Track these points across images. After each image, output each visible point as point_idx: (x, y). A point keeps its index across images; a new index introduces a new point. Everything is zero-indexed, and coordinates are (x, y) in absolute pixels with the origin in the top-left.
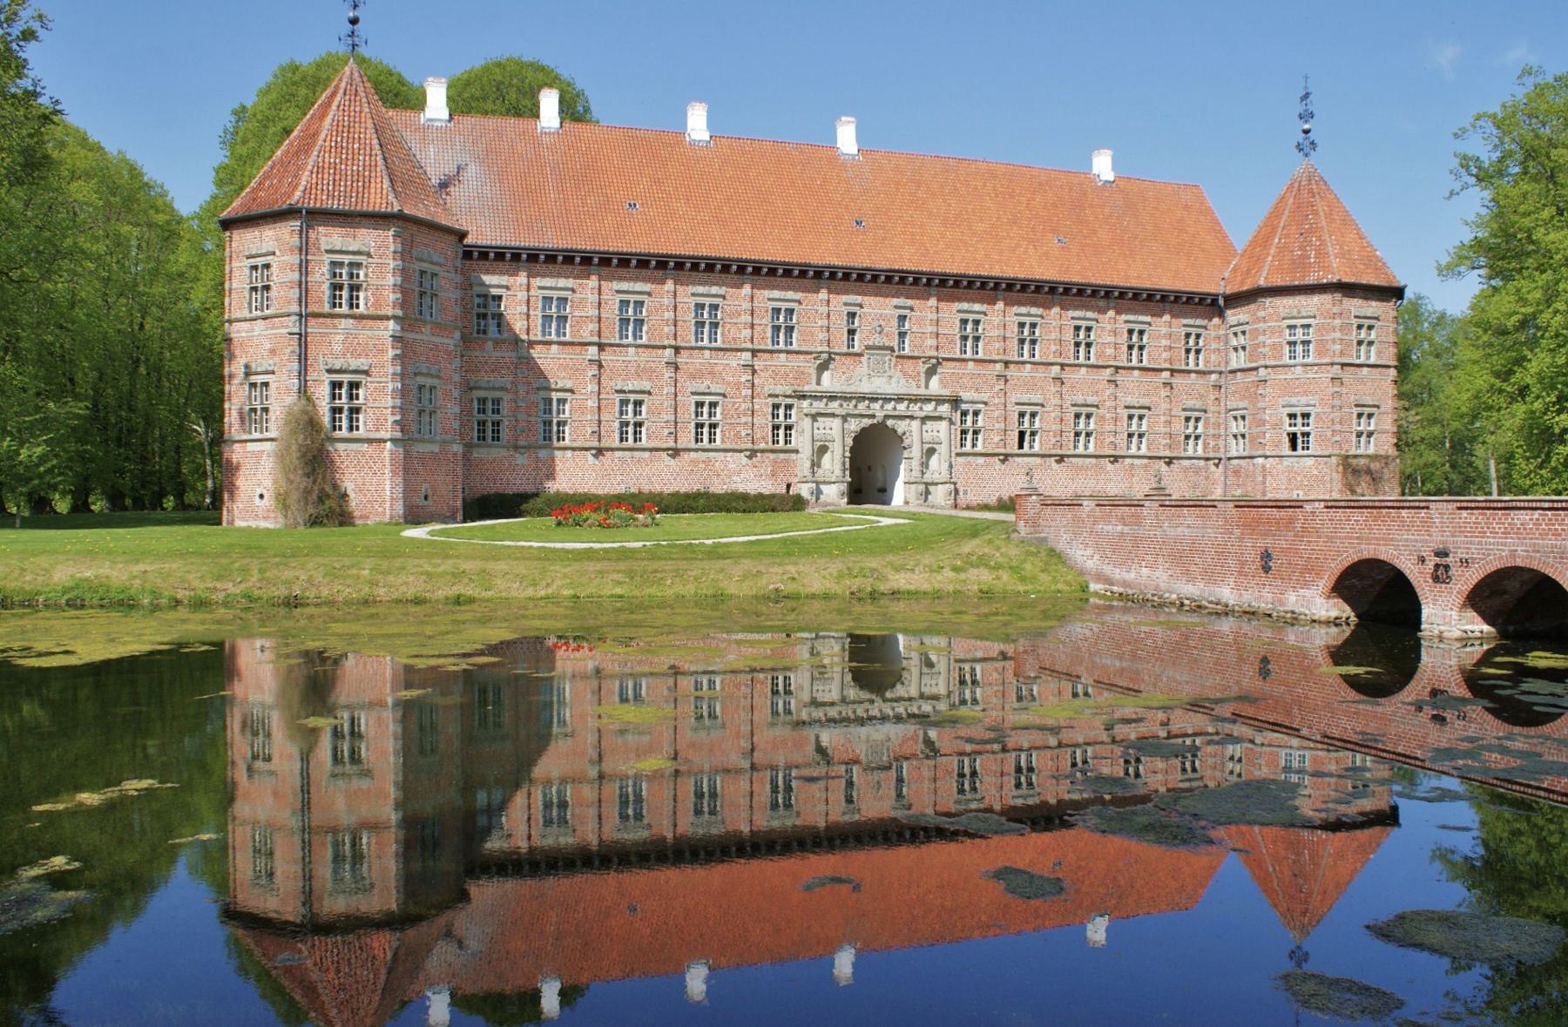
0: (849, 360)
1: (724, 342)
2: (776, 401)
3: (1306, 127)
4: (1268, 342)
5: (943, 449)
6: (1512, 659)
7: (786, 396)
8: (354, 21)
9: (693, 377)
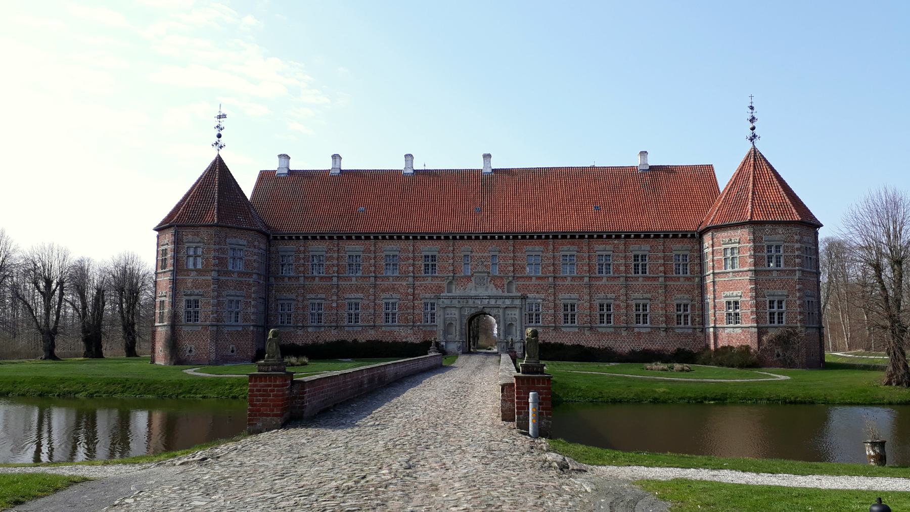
2: (426, 301)
6: (516, 418)
8: (219, 136)
9: (383, 291)
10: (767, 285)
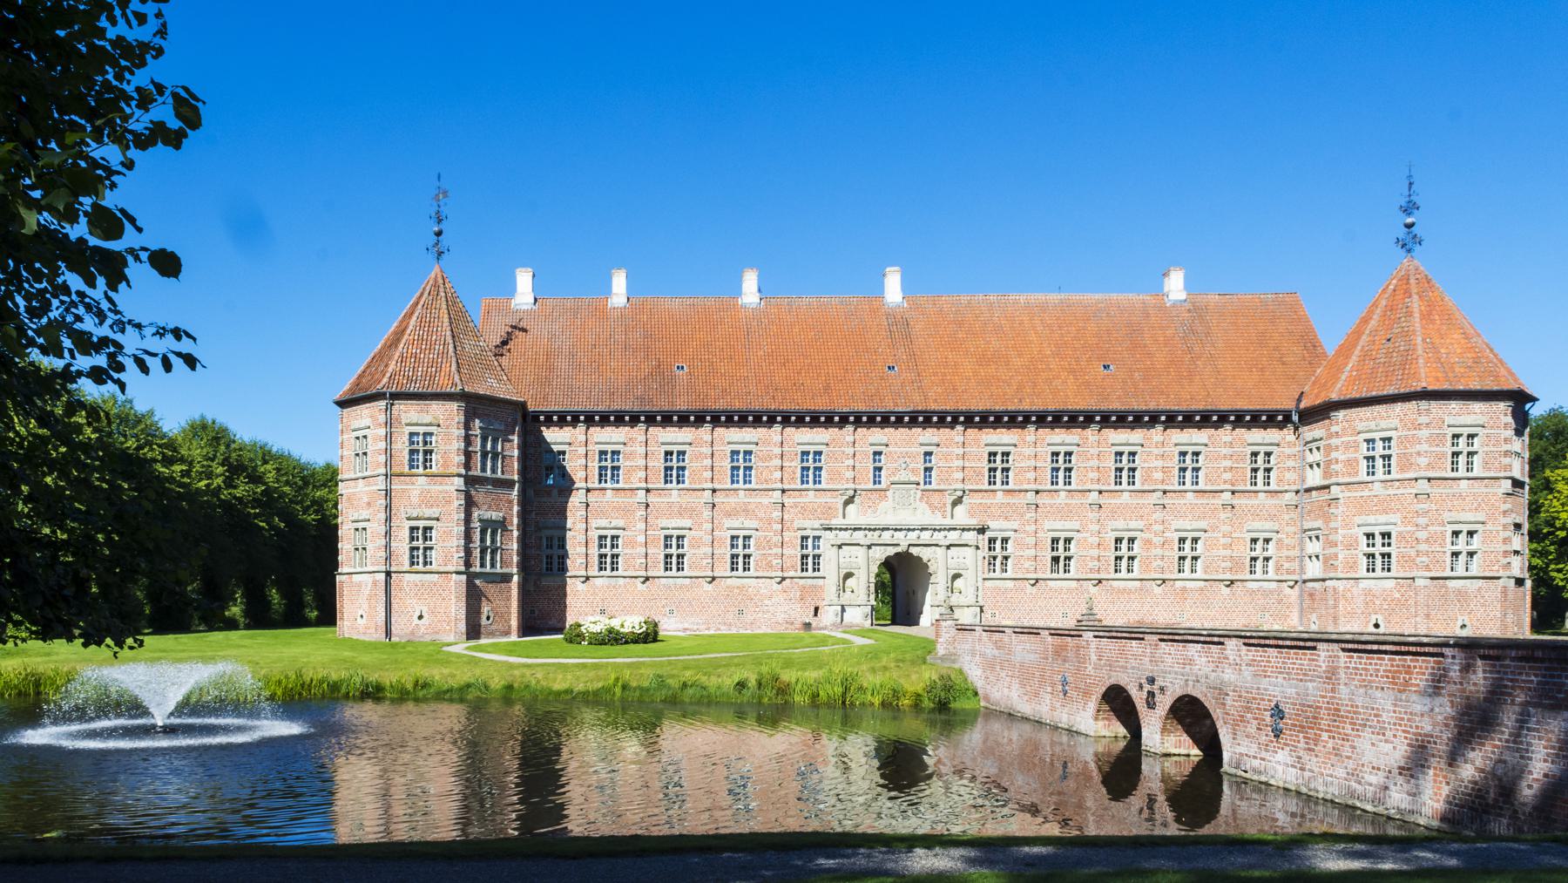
0: (875, 495)
1: (690, 483)
2: (805, 533)
3: (1409, 220)
4: (1342, 457)
5: (968, 575)
7: (813, 529)
8: (439, 234)
9: (729, 515)
10: (1449, 503)
